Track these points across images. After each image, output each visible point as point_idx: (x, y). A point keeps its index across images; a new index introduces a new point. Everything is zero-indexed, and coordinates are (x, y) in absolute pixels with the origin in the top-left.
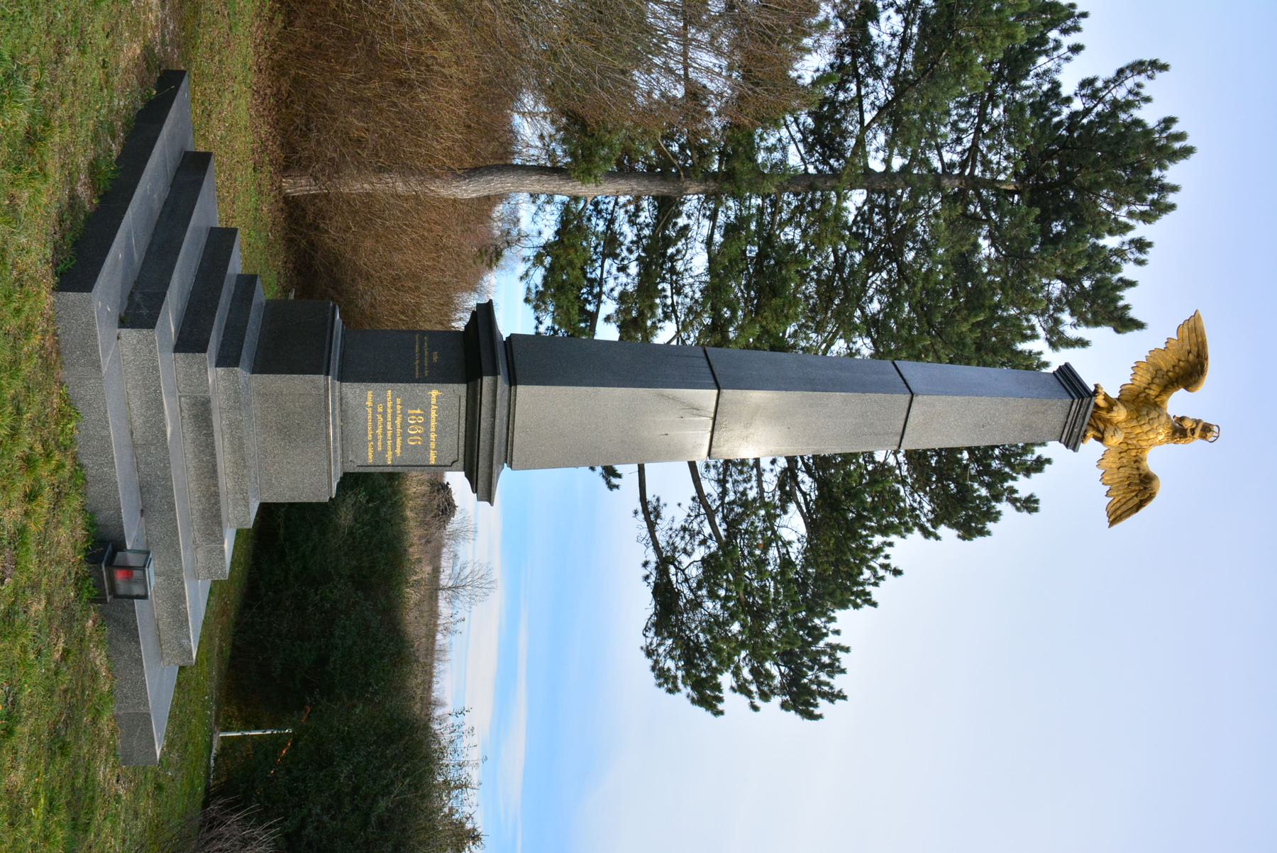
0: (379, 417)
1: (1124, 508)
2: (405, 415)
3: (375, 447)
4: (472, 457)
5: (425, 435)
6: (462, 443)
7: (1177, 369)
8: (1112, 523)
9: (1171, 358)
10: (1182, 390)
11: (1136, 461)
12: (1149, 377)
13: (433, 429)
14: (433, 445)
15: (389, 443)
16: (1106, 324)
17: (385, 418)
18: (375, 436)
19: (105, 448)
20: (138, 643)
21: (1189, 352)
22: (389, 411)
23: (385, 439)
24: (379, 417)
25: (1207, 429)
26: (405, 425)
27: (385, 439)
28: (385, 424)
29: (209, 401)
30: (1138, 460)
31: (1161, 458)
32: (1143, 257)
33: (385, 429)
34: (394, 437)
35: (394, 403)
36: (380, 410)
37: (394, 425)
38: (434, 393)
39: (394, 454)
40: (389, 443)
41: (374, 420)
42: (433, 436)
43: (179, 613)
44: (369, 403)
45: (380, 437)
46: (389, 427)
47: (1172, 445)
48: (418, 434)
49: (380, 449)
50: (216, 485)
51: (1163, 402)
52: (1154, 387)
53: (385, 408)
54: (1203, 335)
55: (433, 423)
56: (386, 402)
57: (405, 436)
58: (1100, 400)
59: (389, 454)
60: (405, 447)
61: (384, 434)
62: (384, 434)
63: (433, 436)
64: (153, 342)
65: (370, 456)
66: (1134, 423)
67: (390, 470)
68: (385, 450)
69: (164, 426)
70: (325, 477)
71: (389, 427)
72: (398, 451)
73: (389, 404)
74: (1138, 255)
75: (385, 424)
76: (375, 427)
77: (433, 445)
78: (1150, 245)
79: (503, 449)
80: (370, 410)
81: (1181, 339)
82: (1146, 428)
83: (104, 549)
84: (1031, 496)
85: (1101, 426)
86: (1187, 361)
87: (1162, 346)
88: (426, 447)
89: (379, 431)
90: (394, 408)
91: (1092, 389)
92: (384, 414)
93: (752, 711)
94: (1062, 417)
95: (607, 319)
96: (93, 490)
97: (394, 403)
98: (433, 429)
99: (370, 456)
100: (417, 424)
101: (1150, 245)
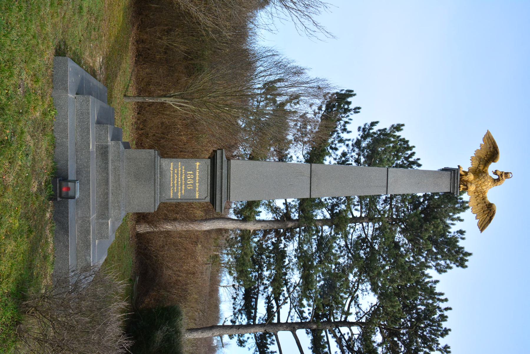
0: (176, 175)
1: (485, 223)
2: (186, 174)
3: (174, 189)
4: (214, 171)
5: (194, 184)
6: (209, 188)
7: (488, 156)
8: (482, 231)
9: (484, 152)
10: (493, 164)
11: (483, 199)
12: (477, 162)
13: (197, 181)
14: (197, 189)
17: (178, 176)
18: (173, 184)
19: (65, 130)
20: (68, 235)
21: (490, 148)
22: (180, 172)
23: (177, 186)
24: (176, 175)
25: (506, 174)
27: (177, 186)
28: (178, 179)
29: (108, 147)
30: (484, 198)
31: (493, 194)
32: (463, 236)
33: (178, 182)
35: (182, 169)
36: (176, 172)
37: (181, 179)
38: (198, 164)
41: (173, 176)
42: (197, 184)
43: (87, 241)
44: (171, 169)
45: (176, 185)
47: (495, 187)
48: (191, 178)
49: (175, 191)
50: (107, 189)
51: (486, 170)
52: (481, 165)
54: (493, 139)
57: (186, 184)
58: (461, 172)
59: (179, 194)
63: (197, 184)
64: (89, 101)
66: (478, 180)
67: (179, 201)
68: (178, 192)
69: (89, 141)
70: (153, 200)
71: (179, 180)
72: (183, 192)
73: (180, 169)
74: (461, 236)
75: (178, 179)
77: (197, 189)
78: (464, 232)
79: (226, 190)
81: (485, 143)
82: (483, 180)
83: (59, 178)
84: (446, 345)
85: (465, 183)
86: (491, 151)
87: (479, 148)
88: (194, 190)
89: (175, 182)
90: (181, 171)
91: (458, 168)
92: (177, 174)
94: (449, 180)
96: (58, 150)
97: (182, 169)
98: (197, 181)
100: (191, 178)
101: (464, 232)
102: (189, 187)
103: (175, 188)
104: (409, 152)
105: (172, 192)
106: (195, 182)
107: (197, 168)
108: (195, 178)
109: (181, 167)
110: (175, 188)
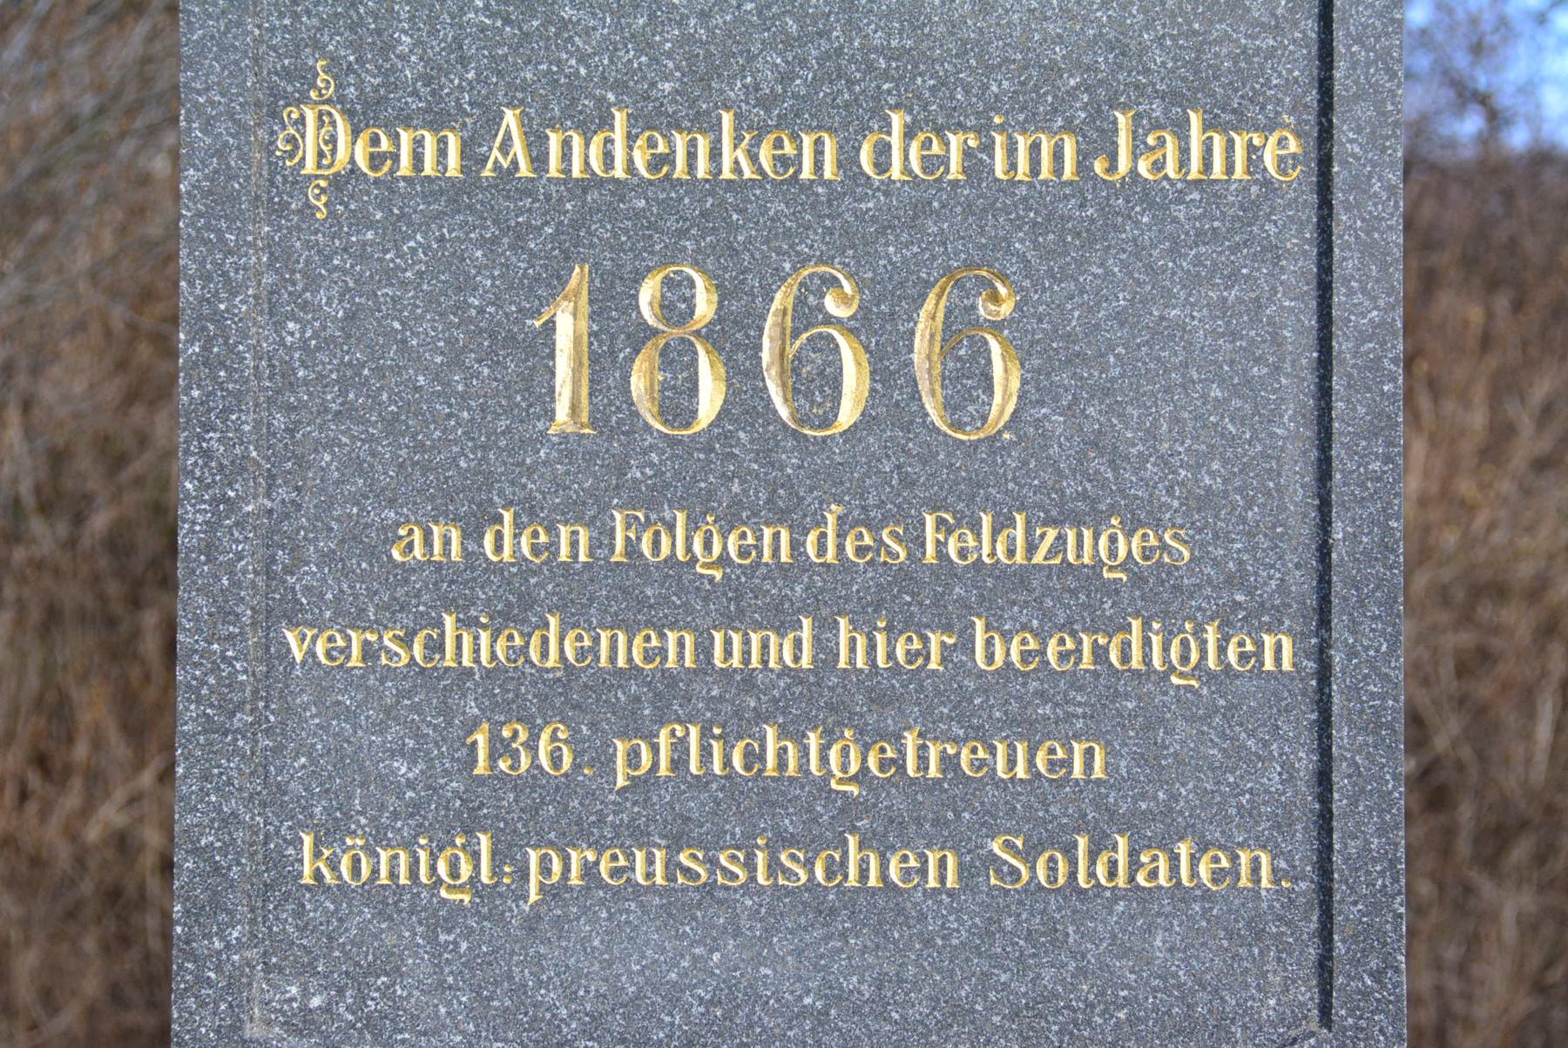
2: (615, 468)
13: (817, 156)
14: (1031, 156)
15: (995, 649)
17: (667, 694)
18: (894, 813)
22: (556, 645)
23: (960, 703)
26: (753, 468)
27: (960, 703)
28: (740, 703)
33: (816, 700)
34: (905, 596)
36: (549, 749)
37: (751, 598)
40: (995, 649)
46: (791, 650)
49: (1088, 760)
53: (516, 694)
57: (902, 466)
68: (1107, 702)
71: (791, 650)
72: (1111, 547)
73: (472, 647)
76: (812, 816)
77: (1031, 156)
89: (840, 761)
90: (515, 600)
95: (83, 678)
98: (817, 156)
100: (734, 336)
102: (967, 379)
103: (1012, 761)
104: (1528, 444)
105: (1106, 866)
106: (842, 219)
107: (436, 154)
108: (709, 221)
110: (1012, 761)
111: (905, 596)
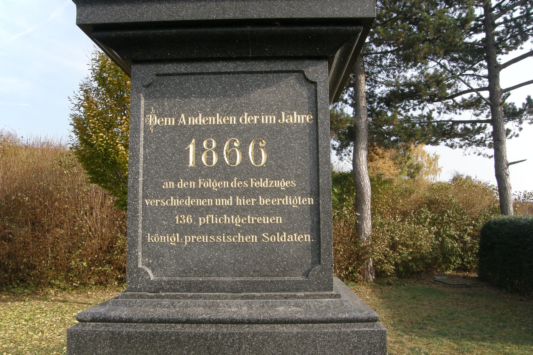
2: (199, 172)
3: (272, 229)
13: (233, 120)
15: (263, 201)
16: (499, 73)
17: (208, 210)
18: (246, 229)
22: (189, 202)
23: (257, 210)
27: (257, 210)
28: (220, 211)
33: (233, 210)
34: (248, 193)
36: (188, 219)
37: (222, 193)
39: (290, 192)
40: (263, 201)
42: (247, 119)
46: (228, 202)
48: (219, 150)
49: (279, 220)
53: (182, 210)
55: (218, 120)
56: (170, 209)
57: (246, 171)
60: (273, 171)
61: (242, 211)
62: (242, 211)
63: (247, 119)
65: (296, 238)
68: (281, 210)
71: (228, 202)
72: (283, 184)
73: (175, 202)
75: (220, 211)
76: (230, 230)
77: (268, 119)
80: (189, 239)
88: (273, 133)
89: (237, 221)
90: (183, 194)
92: (195, 211)
93: (518, 137)
98: (233, 120)
99: (296, 238)
100: (219, 150)
102: (257, 156)
103: (266, 220)
107: (171, 121)
109: (166, 194)
110: (266, 220)
111: (248, 193)
